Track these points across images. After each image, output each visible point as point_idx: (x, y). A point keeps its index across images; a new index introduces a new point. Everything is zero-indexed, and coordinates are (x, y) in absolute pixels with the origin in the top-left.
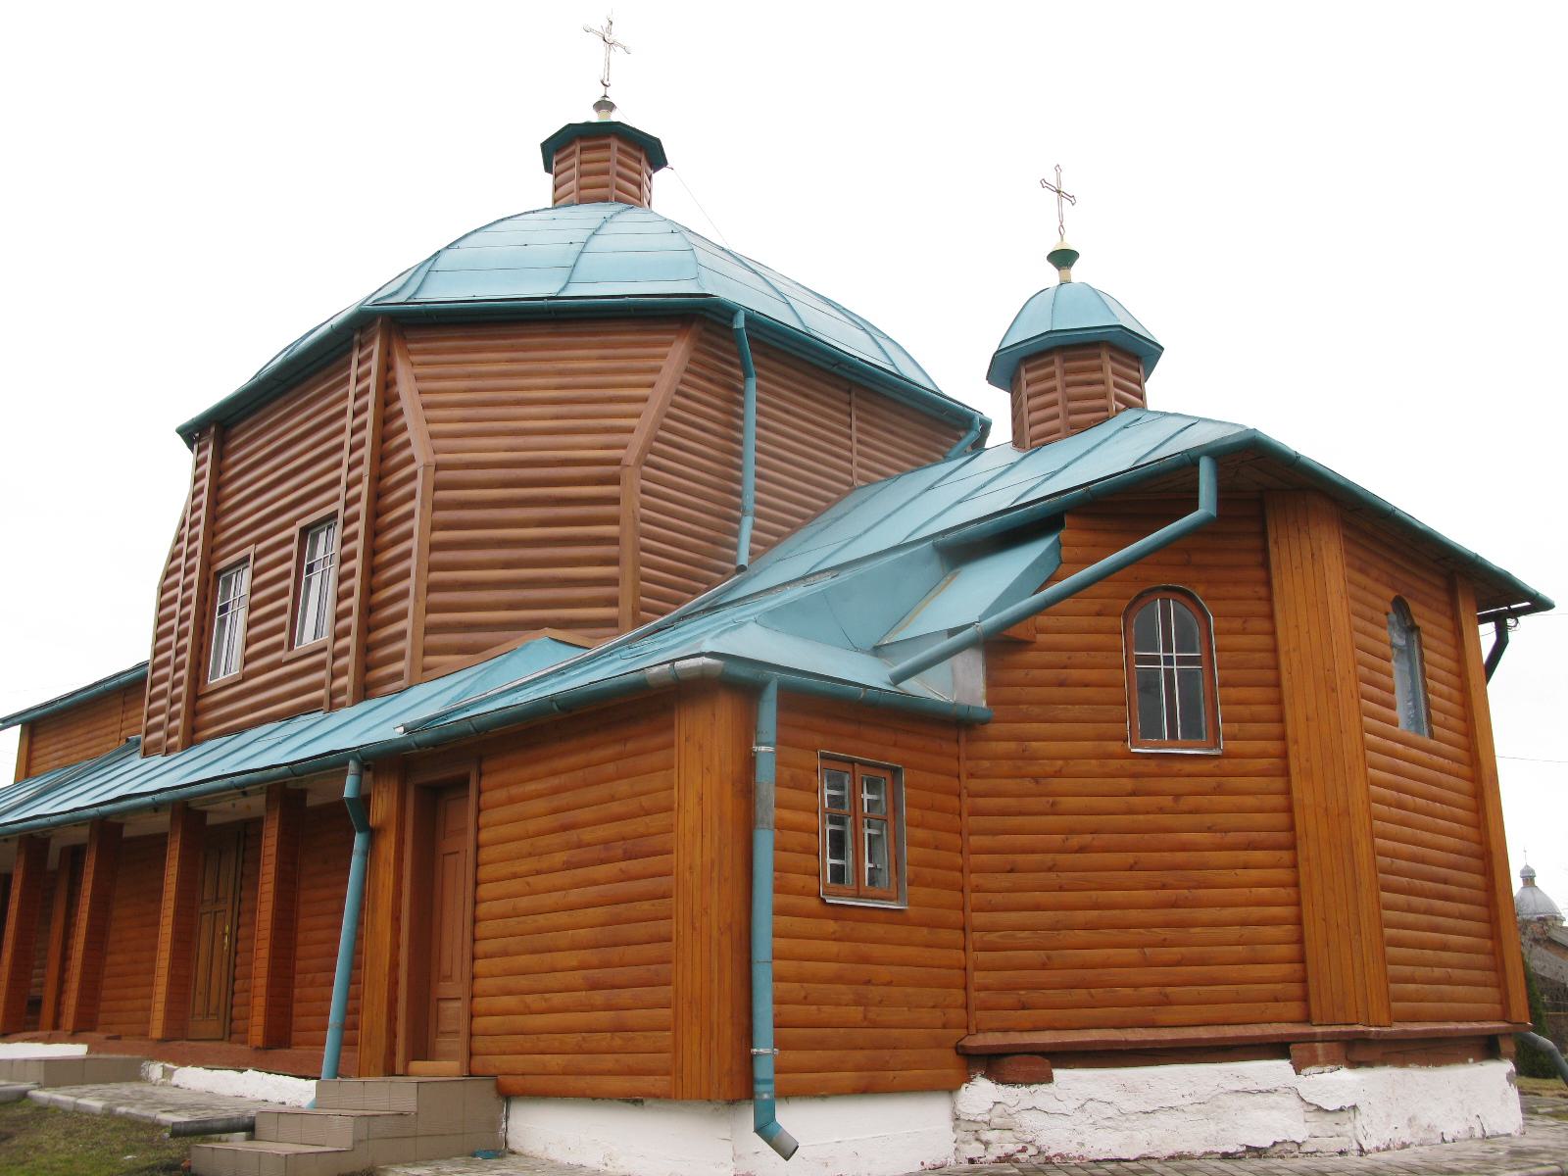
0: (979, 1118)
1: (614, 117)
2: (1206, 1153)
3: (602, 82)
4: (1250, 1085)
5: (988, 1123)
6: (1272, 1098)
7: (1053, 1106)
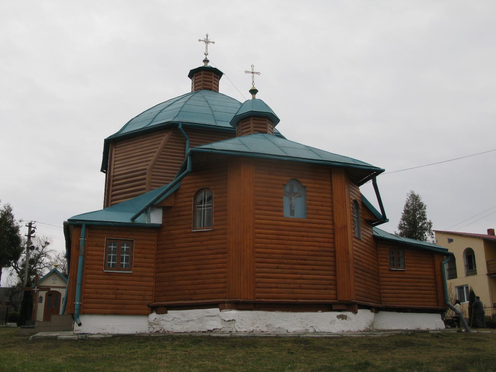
0: (152, 322)
1: (209, 64)
2: (199, 331)
3: (205, 54)
4: (210, 314)
5: (154, 323)
6: (215, 318)
7: (168, 319)
